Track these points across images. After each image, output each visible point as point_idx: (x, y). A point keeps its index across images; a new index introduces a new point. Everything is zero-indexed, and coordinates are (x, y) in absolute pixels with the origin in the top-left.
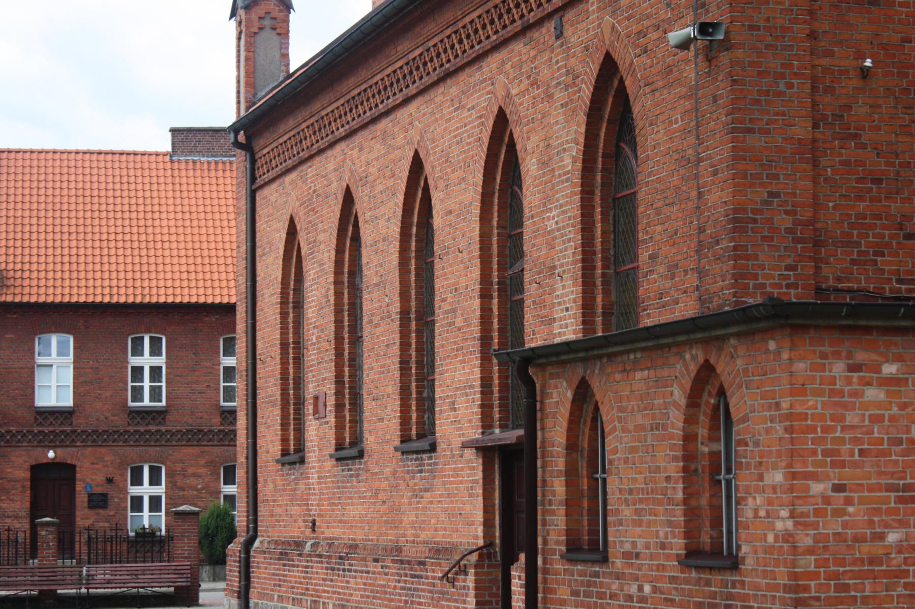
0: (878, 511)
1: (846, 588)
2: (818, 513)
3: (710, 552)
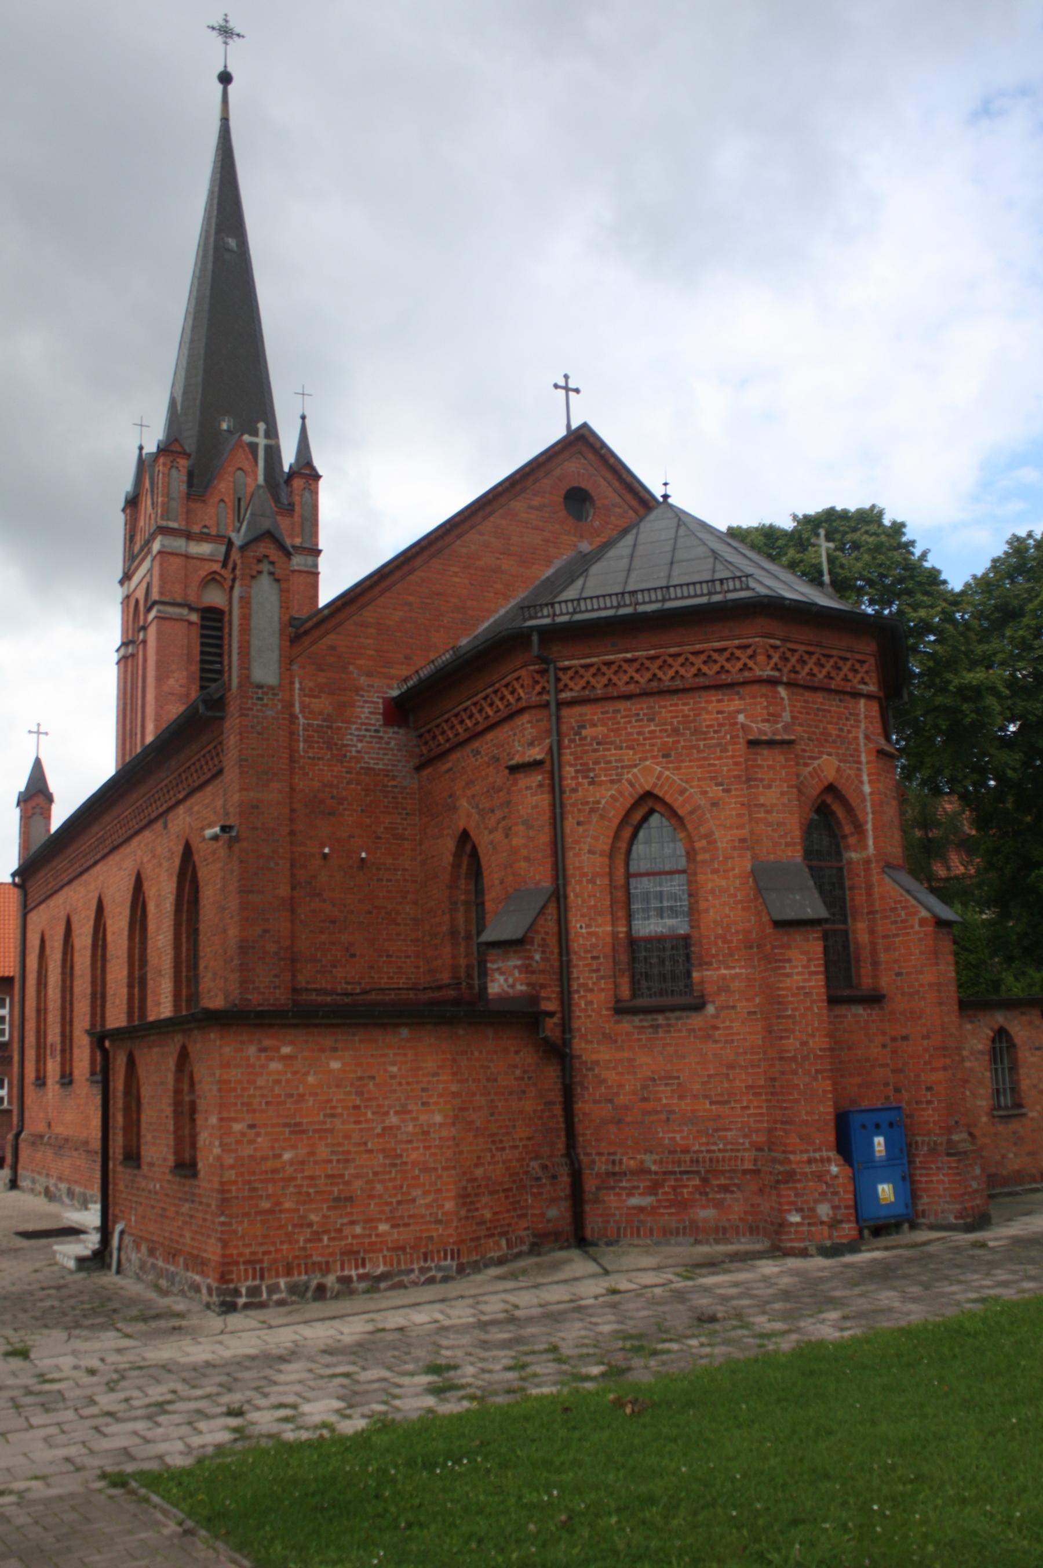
0: (277, 1140)
1: (255, 1189)
2: (237, 1142)
3: (186, 1167)
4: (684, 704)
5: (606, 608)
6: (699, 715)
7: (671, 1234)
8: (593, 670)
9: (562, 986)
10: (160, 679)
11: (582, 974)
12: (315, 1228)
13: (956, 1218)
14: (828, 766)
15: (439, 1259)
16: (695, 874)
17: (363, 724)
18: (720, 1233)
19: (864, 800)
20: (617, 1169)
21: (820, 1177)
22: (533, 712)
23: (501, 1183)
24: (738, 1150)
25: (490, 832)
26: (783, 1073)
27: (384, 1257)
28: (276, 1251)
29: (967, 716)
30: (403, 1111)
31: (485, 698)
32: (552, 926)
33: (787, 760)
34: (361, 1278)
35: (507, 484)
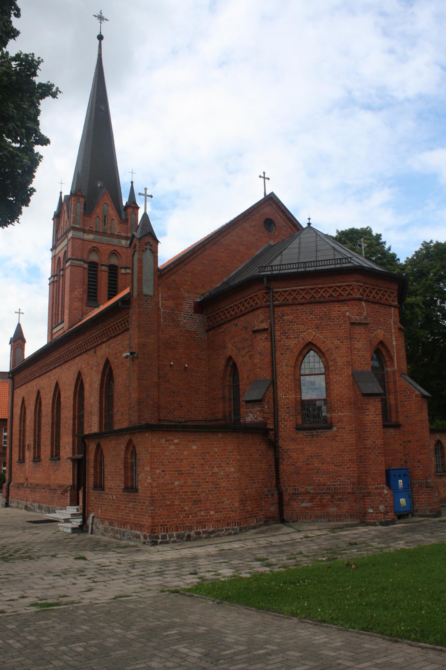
0: (173, 477)
1: (165, 496)
3: (131, 488)
4: (325, 308)
5: (293, 269)
6: (331, 312)
7: (319, 518)
8: (288, 293)
9: (274, 419)
10: (71, 291)
11: (282, 414)
12: (186, 512)
13: (430, 512)
14: (380, 334)
15: (233, 526)
16: (329, 375)
17: (186, 312)
18: (339, 517)
19: (393, 348)
20: (297, 492)
21: (380, 494)
22: (263, 309)
23: (254, 496)
24: (345, 485)
25: (243, 357)
26: (366, 453)
27: (213, 524)
28: (172, 521)
29: (407, 316)
30: (219, 466)
31: (240, 303)
32: (270, 394)
33: (365, 331)
34: (204, 532)
35: (242, 216)
